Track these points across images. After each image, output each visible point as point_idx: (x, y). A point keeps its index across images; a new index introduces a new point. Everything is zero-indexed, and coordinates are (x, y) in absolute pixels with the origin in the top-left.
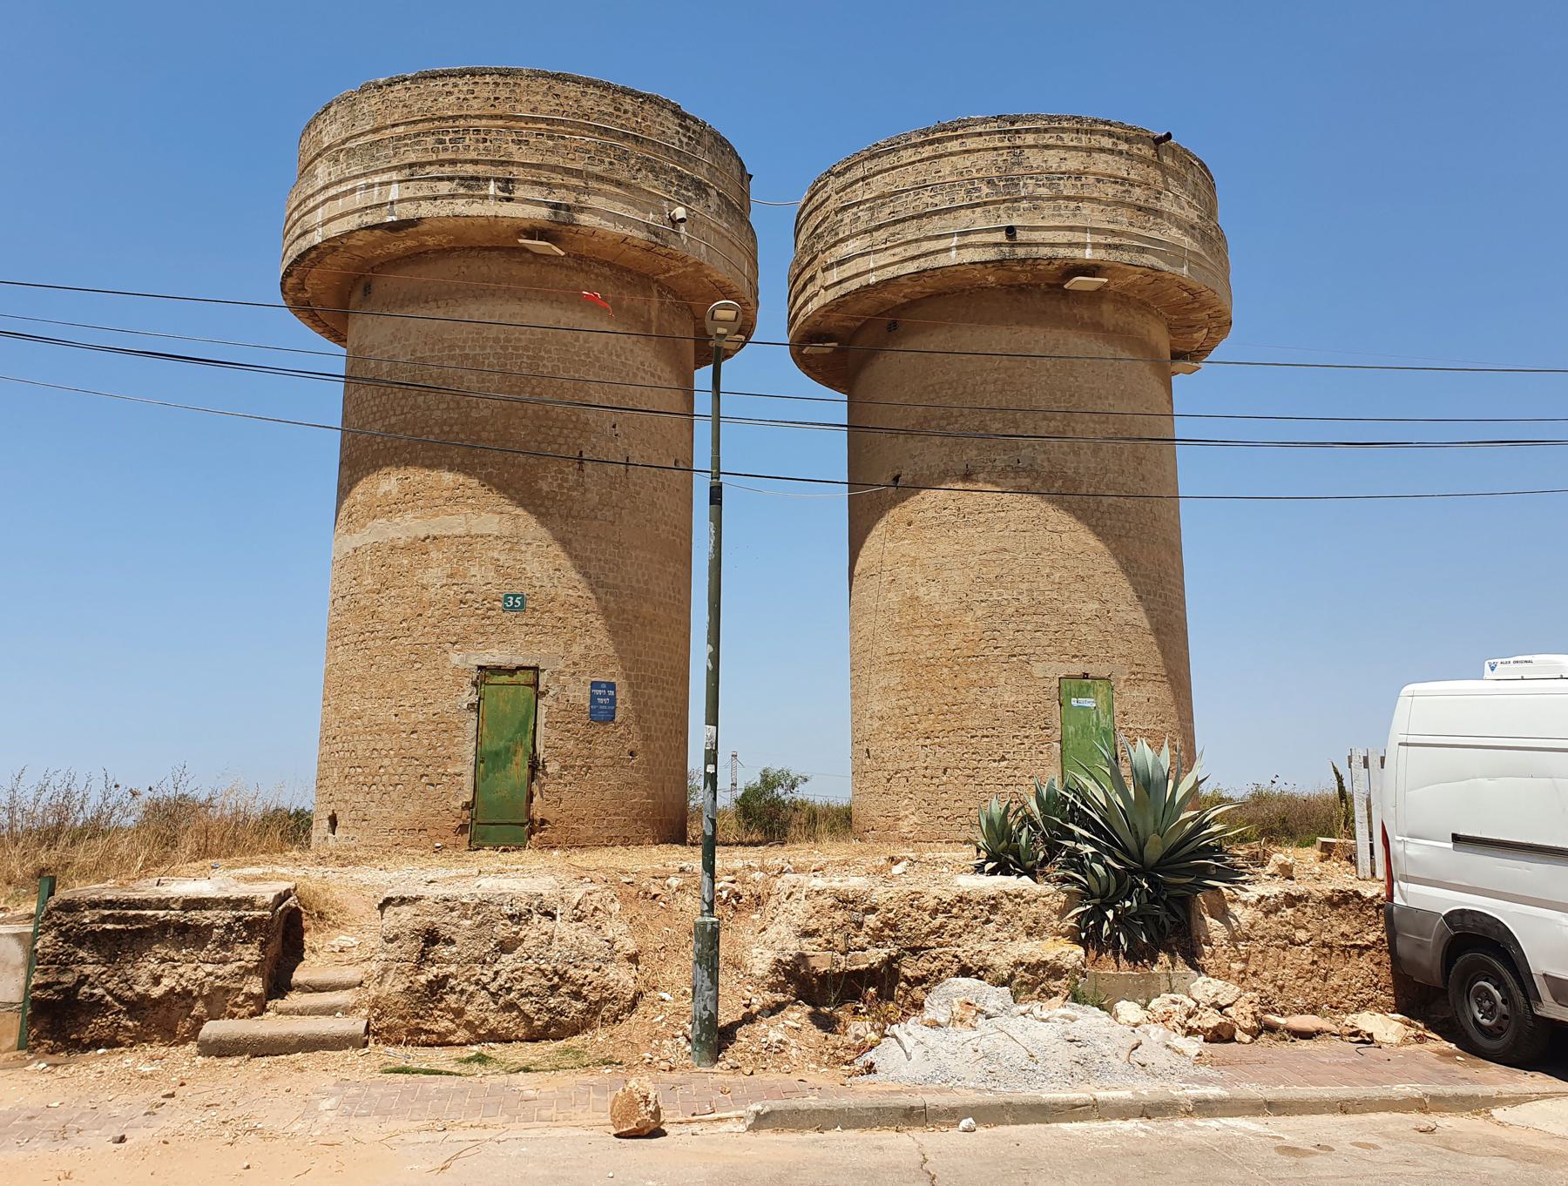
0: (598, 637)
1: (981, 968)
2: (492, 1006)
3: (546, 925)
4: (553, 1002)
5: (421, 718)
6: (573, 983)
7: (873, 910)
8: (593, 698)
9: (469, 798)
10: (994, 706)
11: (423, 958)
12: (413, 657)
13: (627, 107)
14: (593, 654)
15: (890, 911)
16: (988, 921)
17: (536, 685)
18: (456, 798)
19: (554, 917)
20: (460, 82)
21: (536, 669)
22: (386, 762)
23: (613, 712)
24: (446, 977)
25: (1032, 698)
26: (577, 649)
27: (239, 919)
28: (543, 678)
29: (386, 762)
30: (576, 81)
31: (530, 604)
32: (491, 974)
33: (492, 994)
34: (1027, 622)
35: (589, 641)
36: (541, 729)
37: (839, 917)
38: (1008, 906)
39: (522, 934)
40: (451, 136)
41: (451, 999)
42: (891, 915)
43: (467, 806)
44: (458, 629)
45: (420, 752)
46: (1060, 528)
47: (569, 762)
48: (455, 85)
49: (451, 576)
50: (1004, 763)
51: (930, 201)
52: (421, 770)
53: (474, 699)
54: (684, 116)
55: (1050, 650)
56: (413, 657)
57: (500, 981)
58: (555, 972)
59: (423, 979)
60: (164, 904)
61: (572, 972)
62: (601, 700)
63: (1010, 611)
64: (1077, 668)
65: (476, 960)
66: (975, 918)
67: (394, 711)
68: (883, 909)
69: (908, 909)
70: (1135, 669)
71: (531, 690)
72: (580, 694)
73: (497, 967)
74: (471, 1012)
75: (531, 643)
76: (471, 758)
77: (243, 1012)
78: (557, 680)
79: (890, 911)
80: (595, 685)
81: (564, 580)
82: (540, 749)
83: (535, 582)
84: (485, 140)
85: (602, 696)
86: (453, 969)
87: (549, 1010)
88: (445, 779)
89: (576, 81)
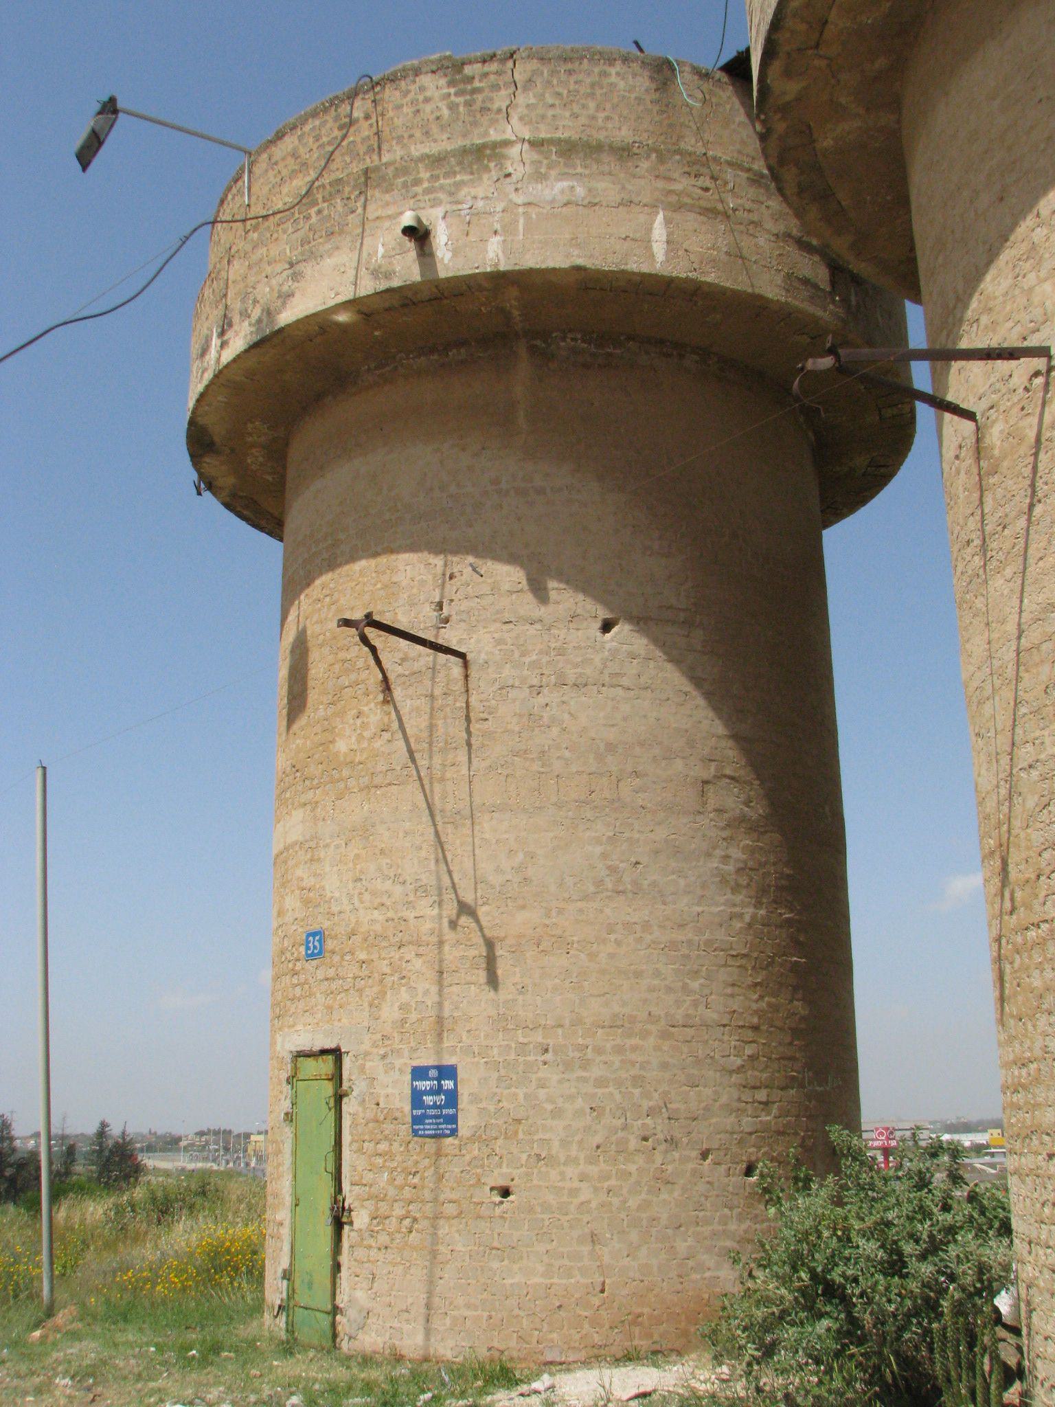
0: (422, 986)
8: (416, 1098)
14: (414, 1016)
23: (453, 1119)
26: (389, 1012)
35: (404, 995)
47: (384, 1208)
54: (459, 66)
62: (429, 1100)
78: (362, 1069)
80: (419, 1073)
81: (367, 897)
83: (335, 909)
85: (432, 1092)
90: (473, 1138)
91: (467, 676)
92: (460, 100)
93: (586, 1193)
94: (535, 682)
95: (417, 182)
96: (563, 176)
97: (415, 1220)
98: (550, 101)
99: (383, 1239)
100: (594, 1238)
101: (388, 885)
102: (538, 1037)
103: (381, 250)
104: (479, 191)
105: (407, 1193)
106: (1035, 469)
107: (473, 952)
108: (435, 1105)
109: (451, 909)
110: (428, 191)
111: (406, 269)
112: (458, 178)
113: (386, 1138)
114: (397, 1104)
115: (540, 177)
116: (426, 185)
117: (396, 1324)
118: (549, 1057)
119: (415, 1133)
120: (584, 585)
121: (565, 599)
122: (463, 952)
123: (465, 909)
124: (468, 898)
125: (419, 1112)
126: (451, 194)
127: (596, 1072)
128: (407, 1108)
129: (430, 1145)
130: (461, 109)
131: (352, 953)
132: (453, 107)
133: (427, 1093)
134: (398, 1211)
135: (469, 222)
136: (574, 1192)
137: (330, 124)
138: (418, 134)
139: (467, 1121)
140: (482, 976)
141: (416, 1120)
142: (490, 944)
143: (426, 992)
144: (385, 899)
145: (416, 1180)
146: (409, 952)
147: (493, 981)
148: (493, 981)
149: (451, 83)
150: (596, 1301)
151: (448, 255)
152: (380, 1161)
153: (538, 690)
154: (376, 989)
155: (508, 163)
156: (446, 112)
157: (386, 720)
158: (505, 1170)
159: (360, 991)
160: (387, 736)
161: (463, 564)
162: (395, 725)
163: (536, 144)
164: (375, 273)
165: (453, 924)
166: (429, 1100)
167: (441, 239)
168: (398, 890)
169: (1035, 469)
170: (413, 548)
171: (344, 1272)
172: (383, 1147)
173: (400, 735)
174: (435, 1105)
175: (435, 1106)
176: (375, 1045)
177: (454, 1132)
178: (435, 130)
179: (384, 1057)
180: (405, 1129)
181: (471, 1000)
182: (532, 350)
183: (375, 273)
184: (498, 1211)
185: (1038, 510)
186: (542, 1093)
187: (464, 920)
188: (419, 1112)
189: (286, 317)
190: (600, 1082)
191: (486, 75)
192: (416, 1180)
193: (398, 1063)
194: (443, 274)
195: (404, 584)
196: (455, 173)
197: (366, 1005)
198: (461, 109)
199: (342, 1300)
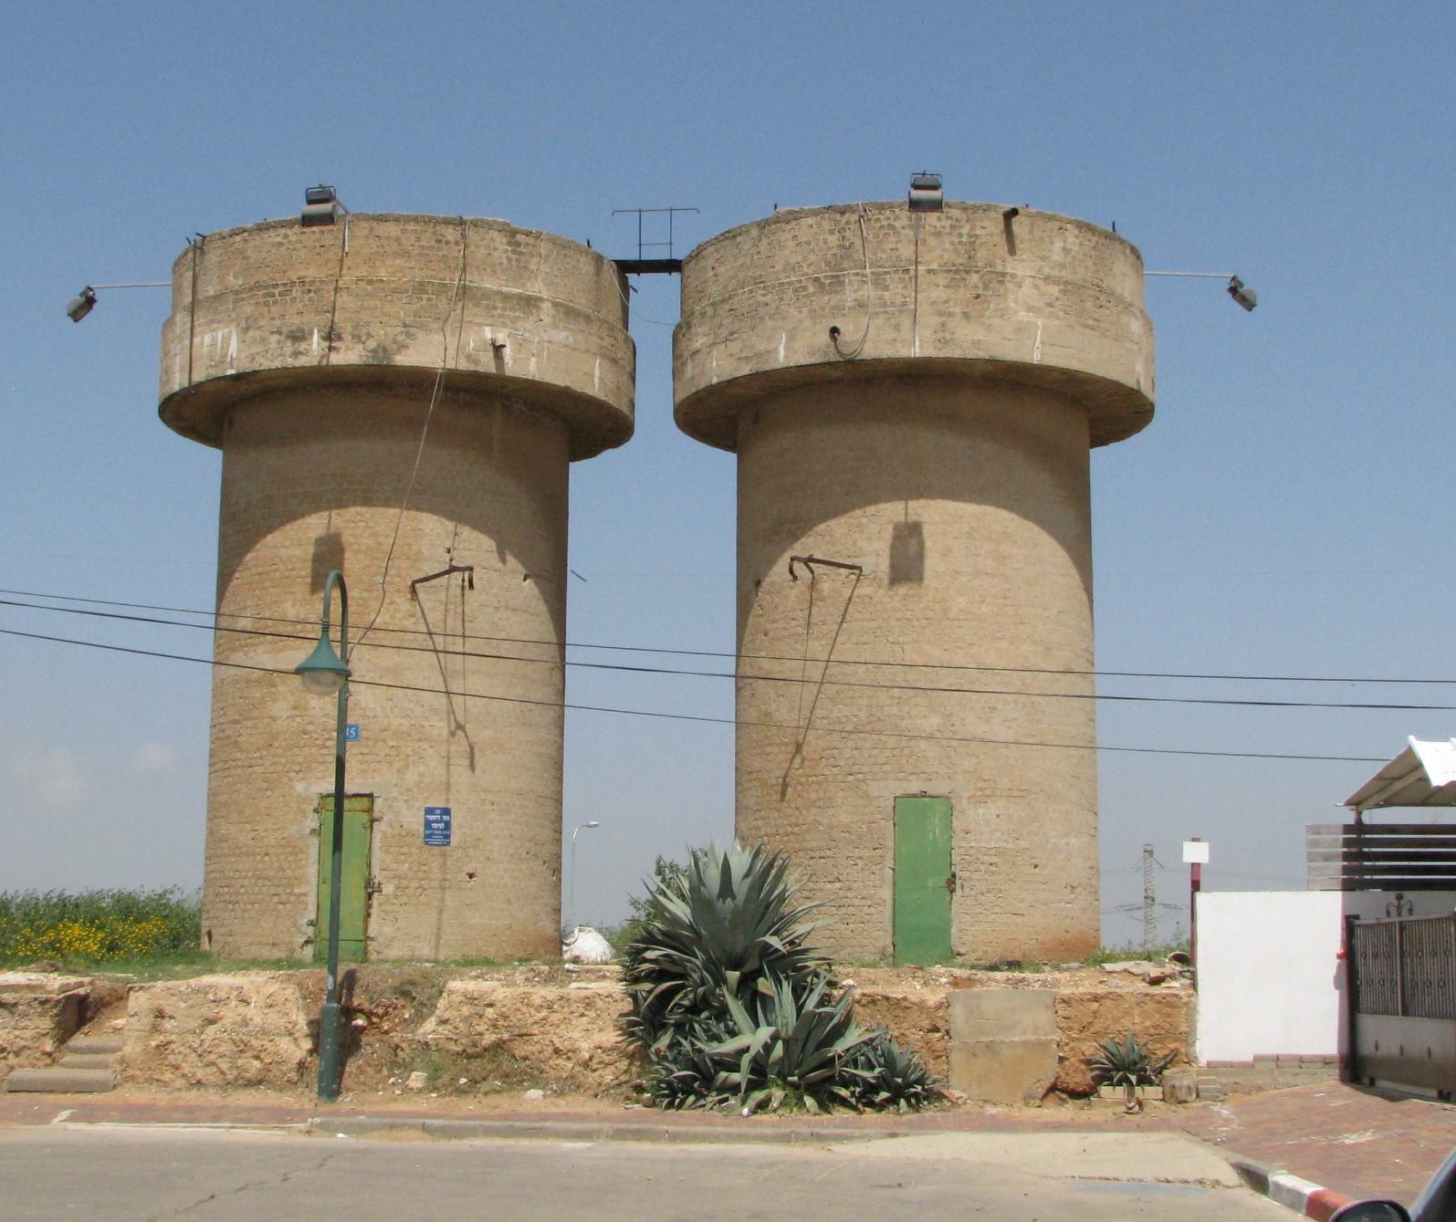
1: (569, 1051)
2: (200, 1064)
3: (242, 1009)
4: (240, 1062)
5: (273, 842)
6: (254, 1050)
7: (491, 1005)
8: (428, 824)
9: (313, 916)
10: (831, 827)
11: (155, 1029)
12: (265, 785)
13: (449, 238)
14: (427, 780)
15: (504, 1006)
16: (583, 1015)
17: (370, 810)
18: (302, 917)
19: (249, 1004)
20: (289, 232)
21: (370, 796)
22: (246, 882)
23: (447, 837)
24: (169, 1043)
25: (867, 818)
27: (36, 999)
28: (378, 804)
29: (246, 882)
30: (397, 220)
31: (364, 734)
32: (198, 1041)
33: (200, 1056)
34: (865, 739)
36: (377, 855)
37: (466, 1010)
38: (600, 1004)
39: (222, 1014)
40: (281, 289)
41: (171, 1058)
42: (504, 1009)
43: (311, 923)
44: (300, 759)
45: (272, 873)
46: (901, 639)
47: (404, 883)
48: (286, 236)
49: (295, 708)
50: (838, 885)
51: (763, 299)
52: (273, 890)
53: (315, 825)
54: (514, 233)
55: (887, 768)
56: (265, 785)
57: (205, 1046)
58: (242, 1041)
59: (153, 1044)
60: (253, 1128)
61: (254, 1042)
62: (435, 825)
64: (915, 786)
65: (189, 1031)
66: (572, 1013)
67: (251, 835)
68: (499, 1005)
69: (519, 1005)
70: (981, 785)
71: (365, 817)
72: (416, 822)
73: (203, 1037)
74: (186, 1068)
75: (365, 771)
76: (314, 880)
77: (41, 1063)
78: (391, 807)
79: (504, 1006)
80: (429, 811)
81: (396, 710)
82: (376, 871)
83: (370, 714)
84: (310, 291)
85: (436, 821)
86: (173, 1037)
87: (238, 1068)
88: (293, 899)
89: (397, 220)
90: (458, 847)
91: (463, 595)
92: (513, 256)
93: (506, 880)
94: (496, 604)
95: (495, 308)
96: (565, 328)
97: (425, 889)
98: (556, 273)
99: (405, 899)
100: (509, 901)
101: (412, 705)
102: (490, 797)
103: (472, 344)
104: (527, 325)
105: (421, 875)
106: (846, 609)
107: (461, 748)
108: (438, 828)
109: (453, 726)
110: (501, 316)
111: (487, 365)
112: (517, 314)
113: (407, 845)
114: (415, 827)
115: (555, 326)
116: (499, 311)
117: (411, 943)
118: (494, 807)
119: (426, 843)
120: (519, 556)
121: (512, 561)
122: (460, 747)
123: (460, 727)
124: (461, 719)
125: (428, 832)
126: (513, 323)
127: (512, 817)
128: (422, 829)
129: (436, 850)
130: (514, 263)
131: (384, 740)
132: (509, 259)
133: (433, 822)
134: (414, 884)
135: (521, 344)
136: (502, 878)
137: (428, 235)
138: (489, 270)
139: (455, 838)
140: (467, 762)
141: (427, 836)
142: (472, 749)
143: (435, 768)
144: (409, 713)
145: (426, 868)
146: (425, 745)
147: (472, 766)
148: (472, 766)
149: (509, 243)
150: (508, 933)
151: (511, 362)
152: (402, 858)
153: (497, 609)
154: (402, 763)
155: (541, 313)
156: (505, 261)
157: (413, 610)
158: (473, 864)
159: (390, 763)
160: (414, 620)
161: (466, 532)
162: (420, 614)
163: (555, 305)
164: (468, 357)
165: (453, 734)
166: (435, 825)
167: (507, 352)
168: (419, 710)
169: (846, 609)
170: (433, 511)
171: (373, 919)
172: (403, 850)
173: (422, 620)
174: (438, 828)
175: (438, 829)
176: (401, 794)
177: (449, 843)
178: (499, 271)
179: (406, 801)
180: (420, 841)
181: (461, 773)
182: (503, 405)
183: (468, 357)
184: (469, 885)
185: (845, 625)
186: (491, 826)
187: (459, 733)
188: (428, 832)
189: (403, 360)
190: (514, 822)
191: (527, 244)
192: (426, 868)
193: (417, 804)
194: (508, 373)
195: (427, 531)
196: (515, 310)
197: (395, 771)
198: (514, 263)
199: (372, 932)
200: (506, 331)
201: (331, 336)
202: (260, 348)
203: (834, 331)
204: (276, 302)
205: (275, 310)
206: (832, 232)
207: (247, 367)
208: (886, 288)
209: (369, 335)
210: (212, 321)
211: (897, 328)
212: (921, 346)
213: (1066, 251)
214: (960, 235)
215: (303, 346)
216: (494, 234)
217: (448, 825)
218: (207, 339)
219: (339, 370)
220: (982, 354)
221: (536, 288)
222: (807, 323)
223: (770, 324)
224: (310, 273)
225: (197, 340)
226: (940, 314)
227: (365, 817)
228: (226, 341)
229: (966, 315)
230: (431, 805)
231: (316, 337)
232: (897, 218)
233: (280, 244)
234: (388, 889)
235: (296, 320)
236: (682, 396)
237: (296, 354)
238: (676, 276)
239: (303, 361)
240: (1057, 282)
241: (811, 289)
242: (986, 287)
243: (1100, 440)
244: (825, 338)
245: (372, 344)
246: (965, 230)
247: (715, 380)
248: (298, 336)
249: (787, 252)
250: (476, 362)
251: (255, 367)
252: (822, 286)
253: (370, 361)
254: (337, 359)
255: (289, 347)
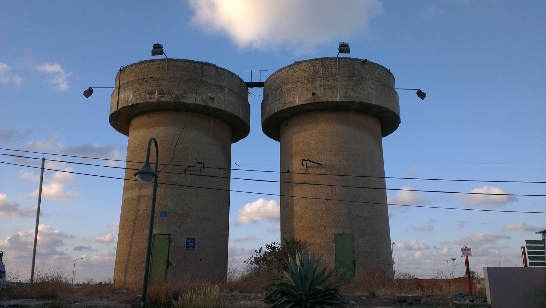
8: (187, 243)
21: (169, 234)
23: (194, 247)
28: (172, 237)
63: (319, 213)
80: (188, 239)
95: (211, 88)
163: (229, 89)
164: (203, 101)
183: (203, 101)
200: (215, 95)
201: (161, 93)
202: (139, 97)
203: (313, 94)
204: (144, 83)
205: (145, 85)
206: (311, 67)
207: (135, 102)
208: (329, 81)
209: (173, 93)
210: (125, 90)
211: (332, 92)
212: (340, 98)
213: (379, 74)
214: (350, 67)
215: (152, 96)
216: (212, 68)
217: (194, 244)
218: (123, 95)
219: (164, 104)
220: (358, 100)
221: (223, 84)
222: (305, 92)
223: (293, 93)
224: (155, 75)
225: (120, 96)
226: (345, 89)
227: (168, 241)
228: (129, 96)
229: (353, 89)
230: (189, 237)
231: (156, 94)
232: (331, 62)
233: (146, 67)
234: (174, 265)
235: (151, 88)
236: (266, 116)
237: (150, 98)
238: (262, 89)
239: (152, 100)
240: (378, 82)
241: (306, 83)
242: (358, 81)
243: (385, 134)
244: (310, 96)
245: (174, 96)
246: (352, 66)
247: (276, 111)
248: (151, 93)
249: (298, 73)
250: (206, 103)
251: (138, 102)
252: (309, 81)
253: (173, 101)
254: (163, 100)
255: (148, 96)
